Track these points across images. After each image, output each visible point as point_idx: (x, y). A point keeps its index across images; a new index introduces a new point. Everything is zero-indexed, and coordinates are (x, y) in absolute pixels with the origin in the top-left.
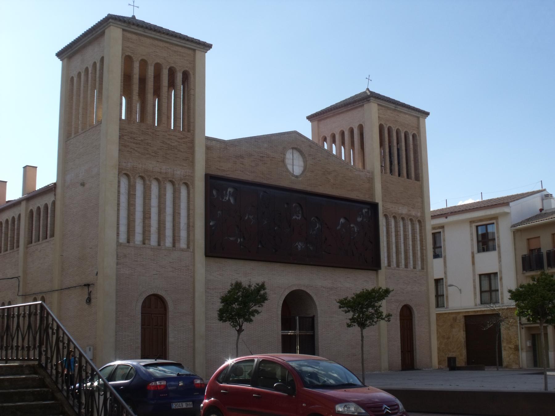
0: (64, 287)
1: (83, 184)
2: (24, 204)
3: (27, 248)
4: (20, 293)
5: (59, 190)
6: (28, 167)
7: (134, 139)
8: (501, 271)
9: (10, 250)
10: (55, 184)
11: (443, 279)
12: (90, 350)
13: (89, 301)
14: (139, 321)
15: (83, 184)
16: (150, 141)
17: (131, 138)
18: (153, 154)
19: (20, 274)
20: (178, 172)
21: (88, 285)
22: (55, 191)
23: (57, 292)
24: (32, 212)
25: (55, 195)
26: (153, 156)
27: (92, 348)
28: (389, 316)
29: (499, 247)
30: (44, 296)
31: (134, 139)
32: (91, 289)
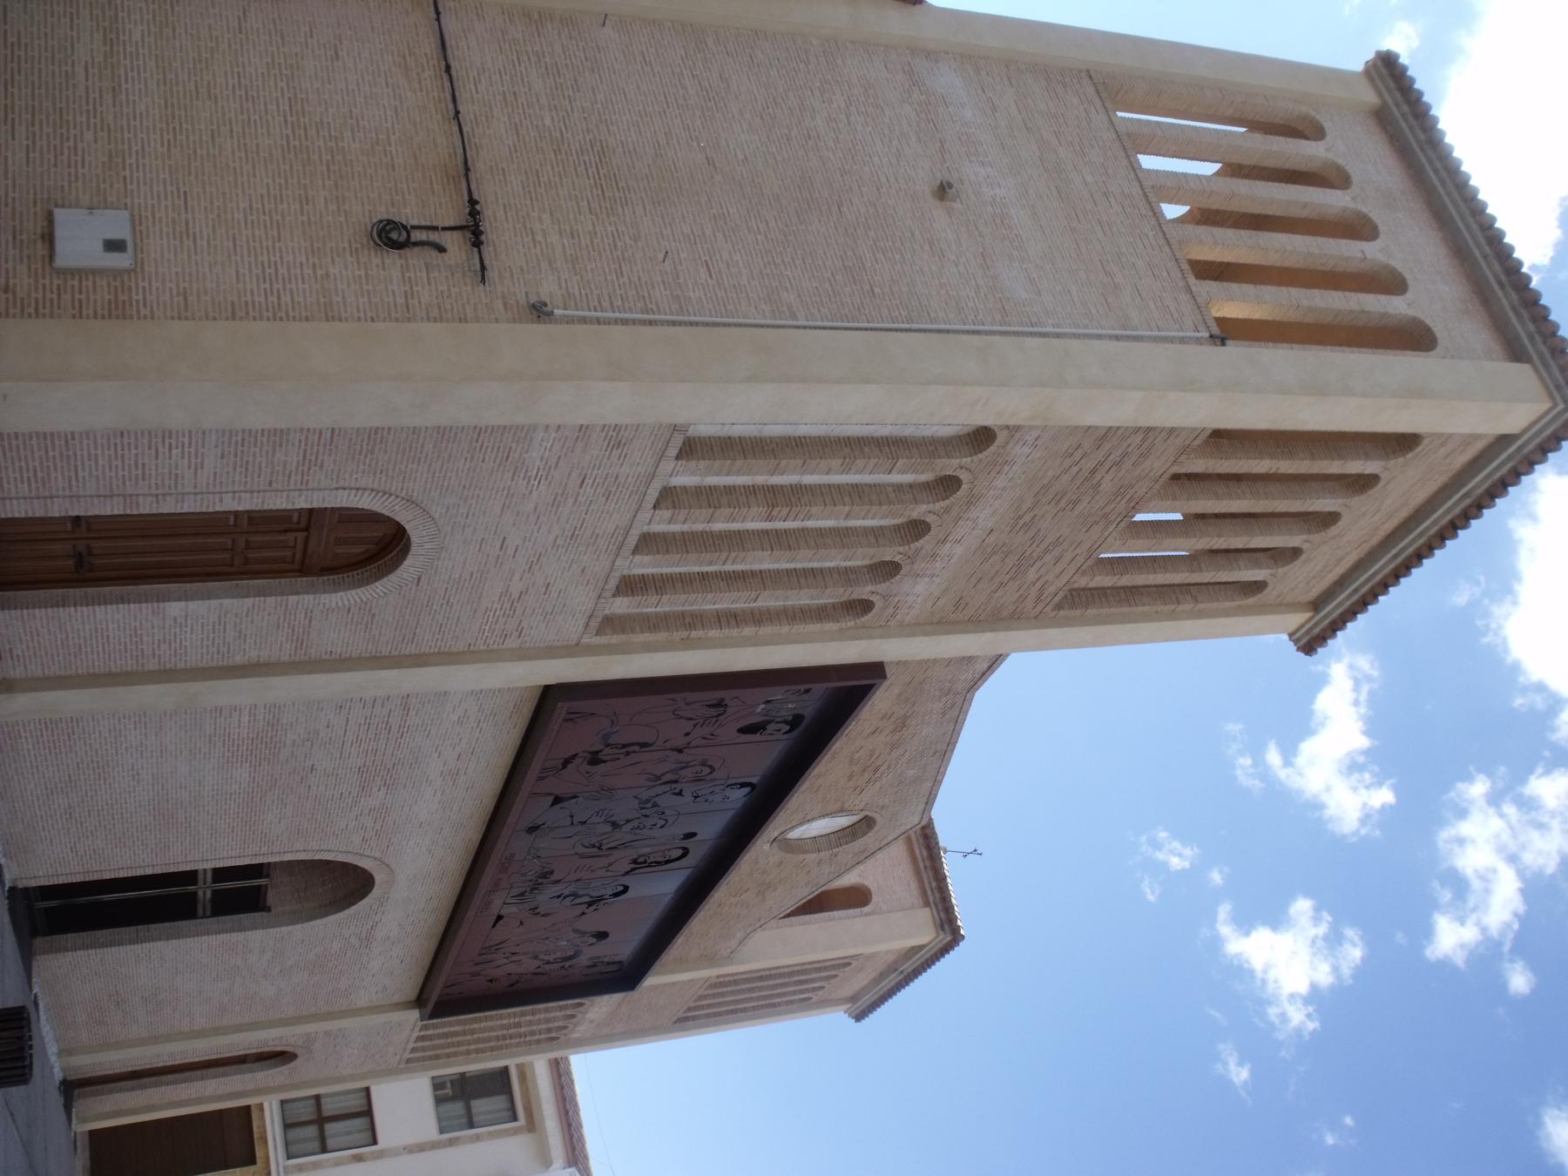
1: (943, 191)
7: (1118, 464)
8: (380, 1155)
11: (375, 1142)
12: (114, 246)
13: (392, 236)
14: (278, 503)
15: (943, 191)
16: (1080, 507)
17: (1124, 455)
18: (1027, 518)
20: (919, 588)
26: (1020, 517)
29: (452, 1142)
31: (1118, 464)
32: (452, 241)
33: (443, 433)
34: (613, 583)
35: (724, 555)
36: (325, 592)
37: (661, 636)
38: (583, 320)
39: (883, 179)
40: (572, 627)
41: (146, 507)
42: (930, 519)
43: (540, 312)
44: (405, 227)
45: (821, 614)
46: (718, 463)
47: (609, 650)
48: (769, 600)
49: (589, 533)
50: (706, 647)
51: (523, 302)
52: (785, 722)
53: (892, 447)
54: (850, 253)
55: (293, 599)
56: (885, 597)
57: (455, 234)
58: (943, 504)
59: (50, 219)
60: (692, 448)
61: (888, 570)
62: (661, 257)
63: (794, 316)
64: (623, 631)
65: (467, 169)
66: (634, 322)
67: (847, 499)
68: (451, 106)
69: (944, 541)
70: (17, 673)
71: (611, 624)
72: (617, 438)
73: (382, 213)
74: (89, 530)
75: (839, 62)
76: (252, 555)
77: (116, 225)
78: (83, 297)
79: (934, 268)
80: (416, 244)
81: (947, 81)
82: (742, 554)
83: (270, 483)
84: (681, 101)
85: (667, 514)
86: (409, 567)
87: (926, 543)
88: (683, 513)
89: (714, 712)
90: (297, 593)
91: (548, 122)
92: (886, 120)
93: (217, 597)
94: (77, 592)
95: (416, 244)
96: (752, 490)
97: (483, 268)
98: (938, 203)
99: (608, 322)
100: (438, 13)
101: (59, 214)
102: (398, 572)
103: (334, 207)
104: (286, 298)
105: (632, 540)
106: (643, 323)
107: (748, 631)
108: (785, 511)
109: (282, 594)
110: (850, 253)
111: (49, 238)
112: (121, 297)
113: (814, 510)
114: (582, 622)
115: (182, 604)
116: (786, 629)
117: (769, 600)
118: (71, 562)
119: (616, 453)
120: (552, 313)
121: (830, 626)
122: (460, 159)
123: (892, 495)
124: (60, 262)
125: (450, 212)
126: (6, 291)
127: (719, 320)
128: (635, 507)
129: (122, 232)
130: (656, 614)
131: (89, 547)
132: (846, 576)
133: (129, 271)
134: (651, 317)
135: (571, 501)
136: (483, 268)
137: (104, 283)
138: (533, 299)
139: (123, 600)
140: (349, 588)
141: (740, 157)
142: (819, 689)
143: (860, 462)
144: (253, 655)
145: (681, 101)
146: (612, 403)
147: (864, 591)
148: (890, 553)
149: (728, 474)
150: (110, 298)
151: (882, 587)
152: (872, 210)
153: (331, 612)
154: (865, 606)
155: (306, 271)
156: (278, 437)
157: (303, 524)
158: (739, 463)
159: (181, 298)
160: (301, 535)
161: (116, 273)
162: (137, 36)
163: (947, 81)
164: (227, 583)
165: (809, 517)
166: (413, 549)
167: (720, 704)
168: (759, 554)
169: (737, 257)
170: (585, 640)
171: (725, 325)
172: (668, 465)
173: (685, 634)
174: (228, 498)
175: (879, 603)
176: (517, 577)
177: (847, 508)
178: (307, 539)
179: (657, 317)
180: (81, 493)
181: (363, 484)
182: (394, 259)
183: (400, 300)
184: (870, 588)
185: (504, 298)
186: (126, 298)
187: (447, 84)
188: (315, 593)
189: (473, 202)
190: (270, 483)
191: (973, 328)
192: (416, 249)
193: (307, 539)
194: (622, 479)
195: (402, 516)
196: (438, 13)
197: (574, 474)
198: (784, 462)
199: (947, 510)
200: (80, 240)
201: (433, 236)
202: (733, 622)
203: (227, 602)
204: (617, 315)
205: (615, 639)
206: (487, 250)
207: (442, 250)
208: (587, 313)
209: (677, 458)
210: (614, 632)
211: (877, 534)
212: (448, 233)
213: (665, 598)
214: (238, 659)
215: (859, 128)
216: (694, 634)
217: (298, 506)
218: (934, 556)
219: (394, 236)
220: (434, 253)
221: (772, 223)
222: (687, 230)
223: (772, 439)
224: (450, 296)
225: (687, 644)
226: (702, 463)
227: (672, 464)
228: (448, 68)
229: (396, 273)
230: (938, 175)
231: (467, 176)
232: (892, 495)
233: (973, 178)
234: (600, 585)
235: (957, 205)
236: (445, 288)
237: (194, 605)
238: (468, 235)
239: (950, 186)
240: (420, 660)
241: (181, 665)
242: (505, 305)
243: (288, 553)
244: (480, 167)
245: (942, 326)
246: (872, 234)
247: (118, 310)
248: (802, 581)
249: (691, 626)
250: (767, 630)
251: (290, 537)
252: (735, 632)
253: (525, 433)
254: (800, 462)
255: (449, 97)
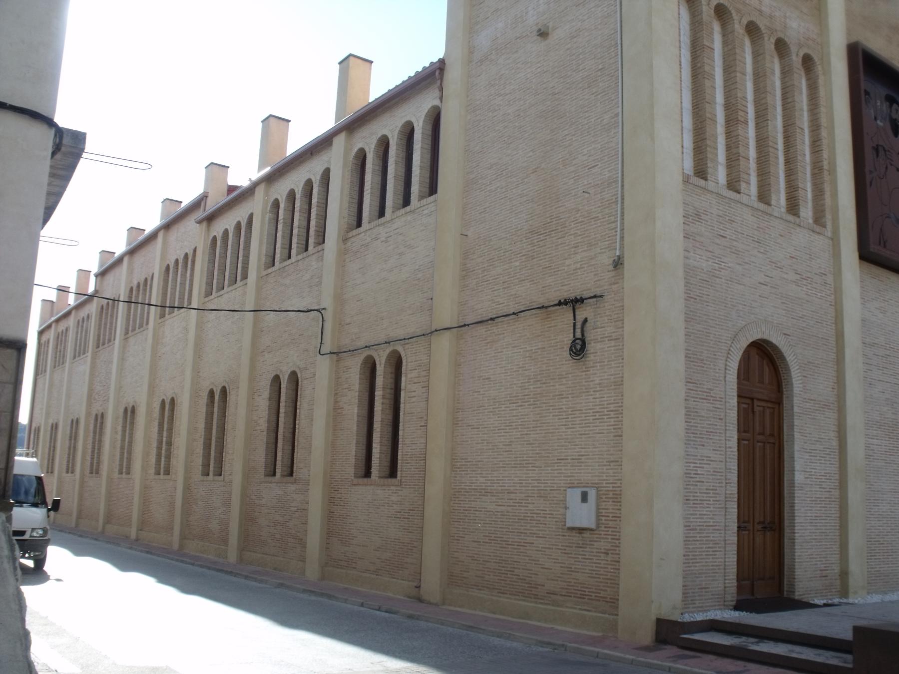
0: (470, 319)
1: (543, 34)
2: (340, 141)
3: (345, 240)
4: (326, 349)
5: (453, 76)
6: (351, 58)
9: (229, 286)
10: (442, 62)
12: (584, 498)
13: (579, 349)
14: (733, 415)
15: (543, 34)
19: (327, 302)
21: (575, 302)
22: (442, 79)
23: (448, 333)
24: (276, 204)
25: (441, 89)
27: (592, 494)
28: (56, 505)
30: (400, 349)
32: (581, 315)
33: (689, 318)
34: (790, 218)
35: (771, 149)
36: (792, 390)
37: (827, 188)
38: (622, 238)
39: (539, 70)
40: (821, 243)
41: (734, 489)
42: (745, 21)
43: (618, 263)
44: (574, 341)
45: (813, 89)
46: (709, 155)
47: (835, 219)
48: (804, 120)
49: (756, 232)
50: (835, 159)
51: (613, 273)
52: (891, 106)
53: (698, 49)
54: (580, 85)
55: (796, 409)
56: (800, 46)
57: (577, 313)
58: (734, 14)
59: (572, 529)
60: (701, 172)
61: (781, 46)
62: (587, 195)
63: (617, 115)
64: (823, 211)
65: (543, 307)
66: (622, 209)
67: (733, 75)
68: (511, 317)
69: (760, 11)
70: (837, 569)
71: (819, 219)
72: (692, 216)
73: (566, 354)
74: (748, 522)
75: (478, 103)
76: (768, 432)
77: (574, 496)
78: (611, 515)
79: (586, 34)
80: (583, 335)
81: (484, 40)
82: (771, 138)
83: (720, 419)
84: (504, 190)
85: (743, 186)
86: (776, 339)
87: (762, 24)
88: (743, 176)
89: (881, 153)
90: (793, 407)
91: (517, 264)
92: (507, 72)
93: (793, 453)
94: (787, 531)
95: (583, 335)
96: (729, 134)
97: (595, 297)
98: (550, 36)
99: (622, 224)
100: (465, 325)
101: (569, 524)
102: (780, 347)
103: (564, 380)
104: (612, 407)
105: (762, 206)
106: (622, 203)
107: (824, 133)
108: (741, 113)
109: (793, 415)
110: (580, 85)
111: (581, 530)
112: (611, 496)
113: (739, 95)
114: (817, 237)
115: (796, 473)
116: (823, 109)
117: (804, 120)
118: (768, 534)
119: (703, 217)
120: (619, 256)
121: (821, 81)
122: (538, 311)
123: (730, 47)
124: (593, 526)
125: (566, 315)
126: (608, 554)
127: (620, 159)
128: (739, 205)
129: (577, 493)
130: (813, 191)
131: (759, 523)
132: (786, 73)
133: (598, 491)
134: (619, 199)
135: (735, 243)
136: (595, 297)
137: (604, 504)
138: (611, 268)
139: (792, 506)
140: (790, 376)
141: (531, 154)
142: (864, 84)
143: (707, 68)
144: (833, 435)
145: (504, 190)
146: (669, 219)
147: (796, 60)
148: (769, 45)
149: (716, 149)
150: (610, 501)
151: (793, 49)
152: (557, 75)
153: (805, 389)
154: (807, 61)
155: (598, 396)
156: (690, 414)
157: (749, 401)
158: (708, 142)
159: (612, 464)
160: (756, 403)
161: (599, 497)
162: (482, 480)
163: (484, 40)
164: (785, 446)
165: (745, 98)
166: (765, 337)
167: (876, 149)
168: (770, 128)
169: (585, 151)
170: (829, 234)
171: (623, 155)
172: (711, 185)
173: (826, 173)
174: (729, 444)
175: (805, 50)
176: (785, 276)
177: (738, 74)
178: (758, 400)
179: (619, 196)
180: (723, 524)
181: (722, 366)
182: (591, 347)
183: (613, 343)
184: (794, 57)
185: (611, 284)
186: (611, 493)
187: (500, 319)
188: (793, 396)
189: (560, 304)
190: (720, 419)
191: (618, 7)
192: (585, 334)
193: (758, 400)
194: (721, 213)
195: (744, 343)
196: (465, 325)
197: (717, 241)
198: (708, 115)
199: (738, 11)
200: (582, 515)
201: (579, 326)
202: (818, 143)
203: (796, 448)
204: (619, 219)
205: (829, 216)
206: (586, 295)
207: (586, 320)
208: (618, 237)
209: (706, 179)
210: (824, 216)
211: (757, 55)
212: (577, 317)
213: (801, 185)
214: (835, 443)
215: (512, 87)
216: (826, 167)
217: (736, 404)
218: (771, 17)
219: (579, 347)
220: (588, 325)
221: (566, 132)
222: (572, 181)
223: (694, 124)
224: (610, 315)
225: (833, 171)
226: (710, 164)
227: (710, 183)
228: (492, 319)
229: (599, 346)
230: (536, 38)
231: (546, 307)
232: (730, 47)
233: (535, 18)
234: (791, 225)
235: (551, 25)
236: (606, 318)
237: (797, 466)
238: (577, 305)
239: (540, 30)
240: (840, 336)
241: (837, 476)
242: (614, 284)
243: (768, 411)
244: (542, 300)
245: (619, 25)
246: (569, 73)
247: (617, 498)
248: (790, 100)
249: (821, 169)
250: (824, 121)
251: (757, 409)
252: (825, 142)
253: (689, 272)
254: (707, 105)
255: (507, 318)
